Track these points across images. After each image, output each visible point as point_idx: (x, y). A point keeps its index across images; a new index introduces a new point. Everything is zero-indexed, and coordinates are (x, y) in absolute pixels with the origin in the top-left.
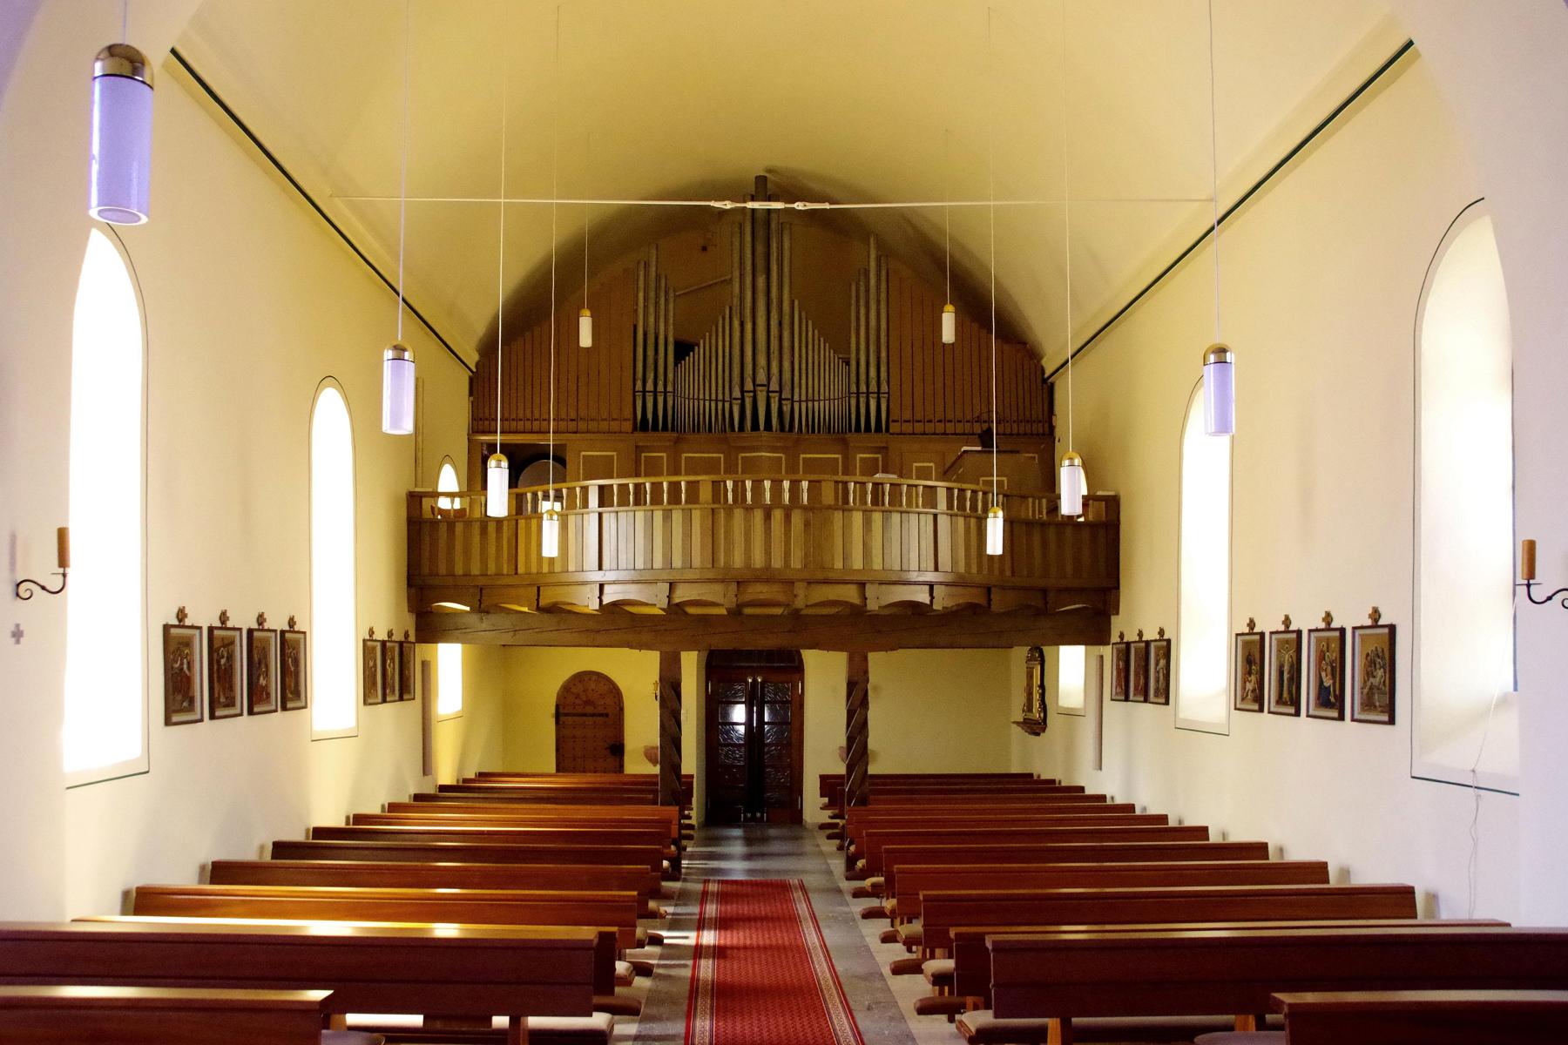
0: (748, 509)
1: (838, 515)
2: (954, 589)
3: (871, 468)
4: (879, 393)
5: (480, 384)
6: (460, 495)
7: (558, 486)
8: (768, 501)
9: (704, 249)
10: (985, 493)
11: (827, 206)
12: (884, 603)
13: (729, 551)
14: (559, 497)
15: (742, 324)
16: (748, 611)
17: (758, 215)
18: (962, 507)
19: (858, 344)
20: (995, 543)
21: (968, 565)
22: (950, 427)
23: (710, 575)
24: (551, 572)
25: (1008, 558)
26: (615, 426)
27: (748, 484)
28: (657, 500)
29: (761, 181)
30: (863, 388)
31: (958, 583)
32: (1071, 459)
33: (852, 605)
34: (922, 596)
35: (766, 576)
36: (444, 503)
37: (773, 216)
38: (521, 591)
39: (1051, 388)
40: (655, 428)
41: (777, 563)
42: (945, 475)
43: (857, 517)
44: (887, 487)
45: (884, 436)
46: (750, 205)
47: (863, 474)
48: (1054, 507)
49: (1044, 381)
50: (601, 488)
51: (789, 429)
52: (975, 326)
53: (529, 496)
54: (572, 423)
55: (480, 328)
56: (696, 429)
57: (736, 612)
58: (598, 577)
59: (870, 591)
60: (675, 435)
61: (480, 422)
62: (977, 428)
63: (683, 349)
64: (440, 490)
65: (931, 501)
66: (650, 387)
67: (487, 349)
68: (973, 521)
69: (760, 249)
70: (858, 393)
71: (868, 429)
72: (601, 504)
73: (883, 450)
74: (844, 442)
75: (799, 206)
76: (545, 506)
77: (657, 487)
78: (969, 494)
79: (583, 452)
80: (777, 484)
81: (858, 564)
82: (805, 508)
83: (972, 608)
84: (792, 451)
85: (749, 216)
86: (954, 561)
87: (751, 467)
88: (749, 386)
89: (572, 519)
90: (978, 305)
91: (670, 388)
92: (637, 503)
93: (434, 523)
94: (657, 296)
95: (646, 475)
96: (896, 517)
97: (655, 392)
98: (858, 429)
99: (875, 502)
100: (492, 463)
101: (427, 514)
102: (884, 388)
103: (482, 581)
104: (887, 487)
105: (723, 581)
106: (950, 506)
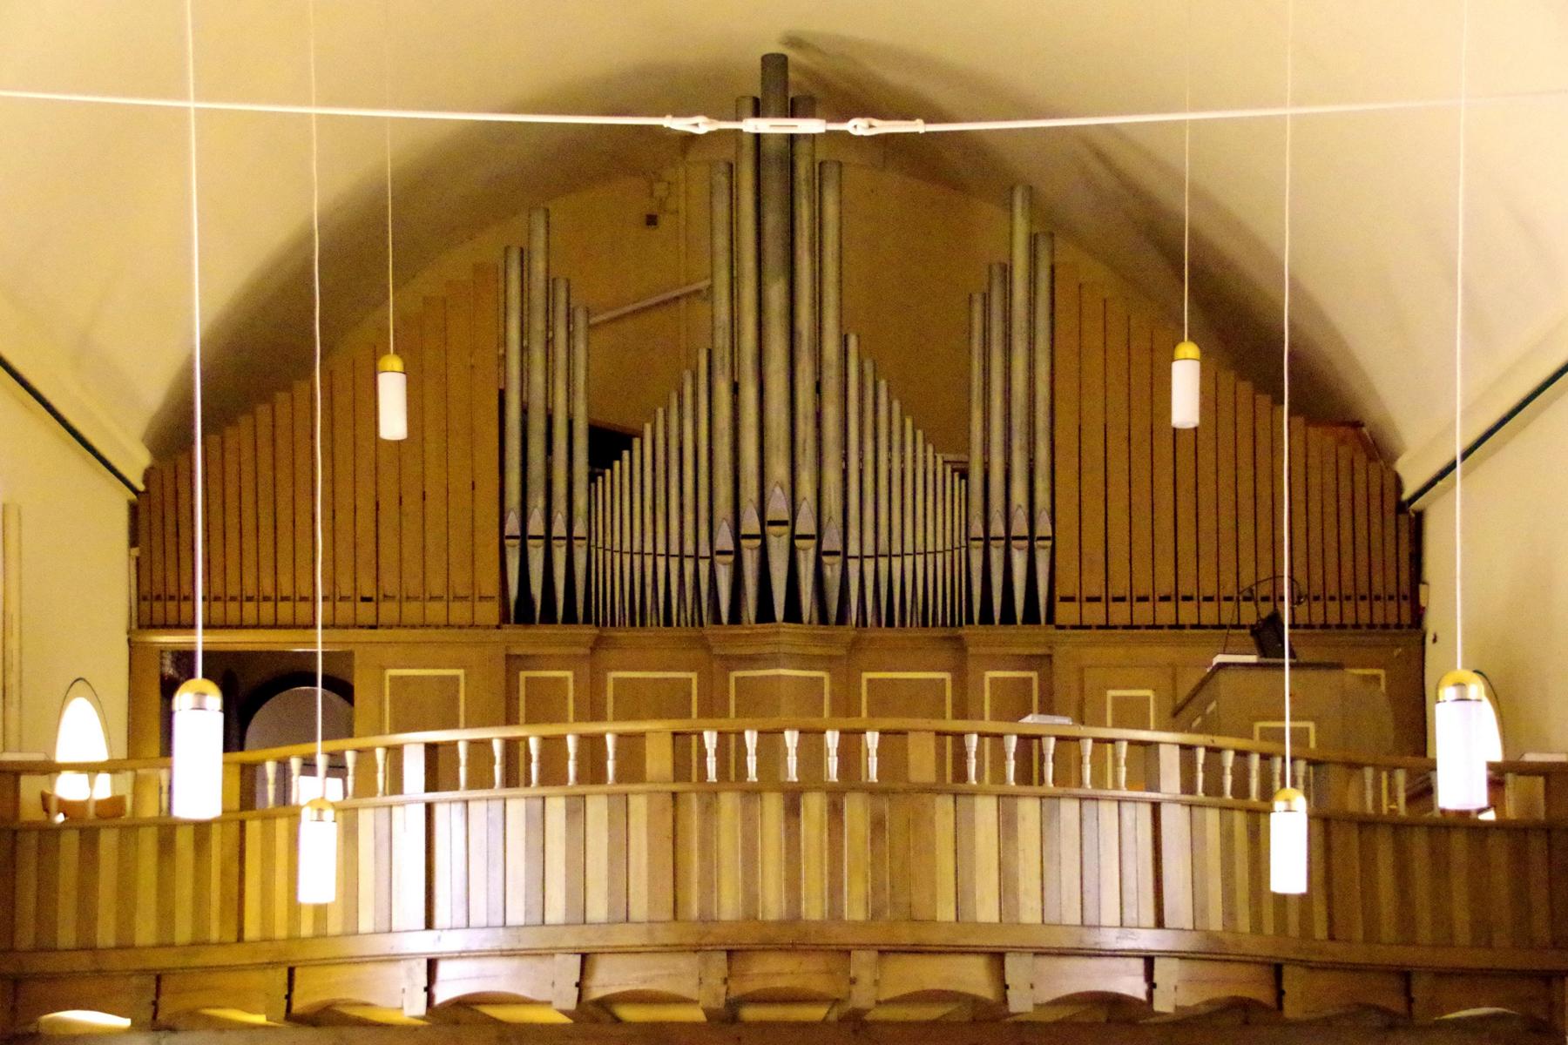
0: (752, 793)
1: (944, 804)
2: (1197, 965)
3: (1015, 703)
4: (1031, 537)
5: (153, 518)
6: (111, 767)
7: (334, 745)
8: (793, 776)
9: (652, 220)
10: (1266, 757)
11: (918, 127)
12: (1049, 997)
13: (710, 885)
14: (336, 767)
15: (735, 389)
16: (750, 1013)
17: (769, 148)
18: (1213, 788)
19: (986, 435)
20: (1289, 870)
21: (1230, 914)
22: (1188, 613)
23: (665, 936)
24: (321, 935)
25: (1319, 910)
26: (460, 612)
27: (751, 738)
28: (592, 771)
29: (775, 65)
30: (998, 528)
31: (1210, 954)
32: (1460, 685)
33: (976, 1001)
34: (1131, 984)
35: (793, 939)
36: (70, 788)
37: (802, 148)
38: (256, 978)
39: (1418, 521)
40: (549, 617)
41: (814, 909)
42: (1176, 716)
43: (986, 809)
44: (1050, 744)
45: (1042, 631)
46: (751, 125)
47: (997, 716)
48: (1424, 790)
49: (1402, 507)
50: (431, 748)
51: (836, 615)
52: (1245, 388)
53: (271, 768)
54: (367, 607)
55: (153, 394)
56: (637, 617)
57: (726, 1017)
58: (427, 943)
59: (1016, 969)
60: (589, 631)
61: (156, 603)
62: (1249, 614)
63: (608, 445)
64: (60, 758)
65: (1145, 774)
66: (536, 526)
67: (170, 441)
68: (1240, 819)
69: (773, 220)
70: (987, 539)
71: (1008, 617)
72: (431, 785)
73: (1043, 662)
74: (959, 644)
75: (858, 127)
76: (305, 789)
77: (553, 747)
78: (1229, 758)
79: (385, 671)
80: (811, 737)
81: (987, 910)
82: (871, 791)
83: (1240, 1007)
84: (845, 666)
85: (748, 146)
86: (1199, 909)
87: (755, 701)
88: (751, 524)
89: (366, 819)
90: (1260, 349)
91: (580, 529)
92: (510, 780)
93: (49, 833)
94: (549, 327)
95: (531, 720)
96: (1069, 809)
97: (548, 538)
98: (987, 618)
99: (1025, 776)
100: (183, 700)
101: (30, 810)
102: (1043, 528)
103: (163, 960)
104: (1050, 744)
105: (696, 949)
106: (1188, 786)
